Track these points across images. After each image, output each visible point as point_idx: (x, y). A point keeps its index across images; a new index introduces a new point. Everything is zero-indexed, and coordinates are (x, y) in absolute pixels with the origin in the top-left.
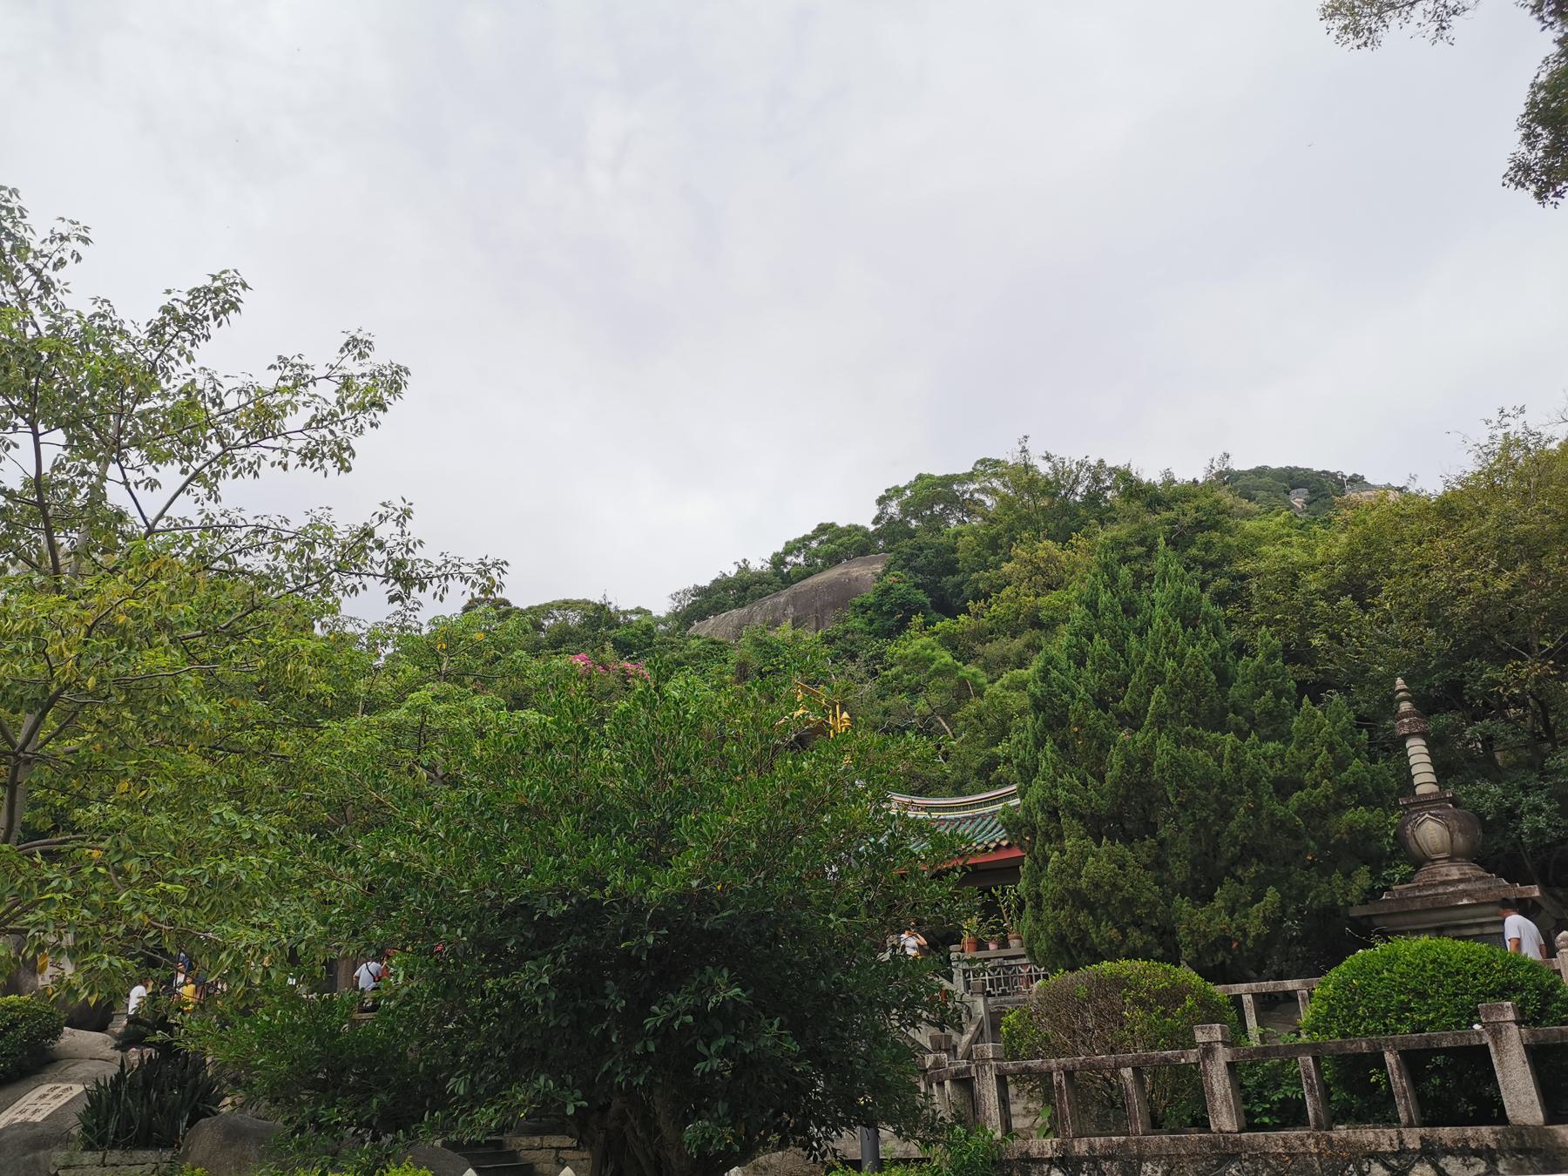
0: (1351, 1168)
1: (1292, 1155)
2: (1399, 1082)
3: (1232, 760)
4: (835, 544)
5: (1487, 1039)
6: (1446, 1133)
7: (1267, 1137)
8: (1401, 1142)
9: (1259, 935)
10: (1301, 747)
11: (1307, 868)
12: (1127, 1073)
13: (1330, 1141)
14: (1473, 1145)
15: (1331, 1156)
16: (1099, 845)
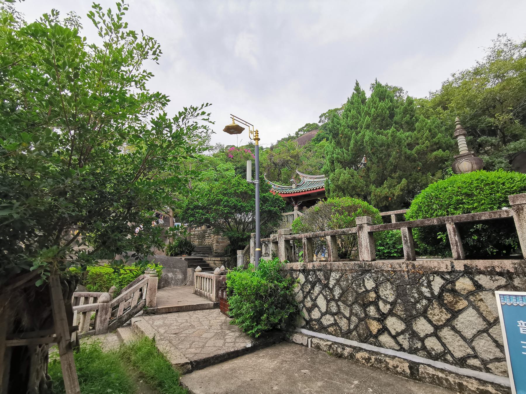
0: (424, 278)
1: (394, 271)
2: (453, 238)
3: (392, 136)
4: (310, 127)
5: (513, 213)
6: (481, 264)
7: (383, 263)
8: (452, 267)
9: (398, 195)
10: (419, 131)
11: (418, 172)
12: (329, 238)
13: (413, 266)
14: (498, 270)
15: (413, 273)
16: (345, 169)
